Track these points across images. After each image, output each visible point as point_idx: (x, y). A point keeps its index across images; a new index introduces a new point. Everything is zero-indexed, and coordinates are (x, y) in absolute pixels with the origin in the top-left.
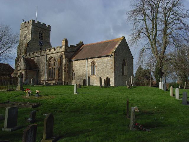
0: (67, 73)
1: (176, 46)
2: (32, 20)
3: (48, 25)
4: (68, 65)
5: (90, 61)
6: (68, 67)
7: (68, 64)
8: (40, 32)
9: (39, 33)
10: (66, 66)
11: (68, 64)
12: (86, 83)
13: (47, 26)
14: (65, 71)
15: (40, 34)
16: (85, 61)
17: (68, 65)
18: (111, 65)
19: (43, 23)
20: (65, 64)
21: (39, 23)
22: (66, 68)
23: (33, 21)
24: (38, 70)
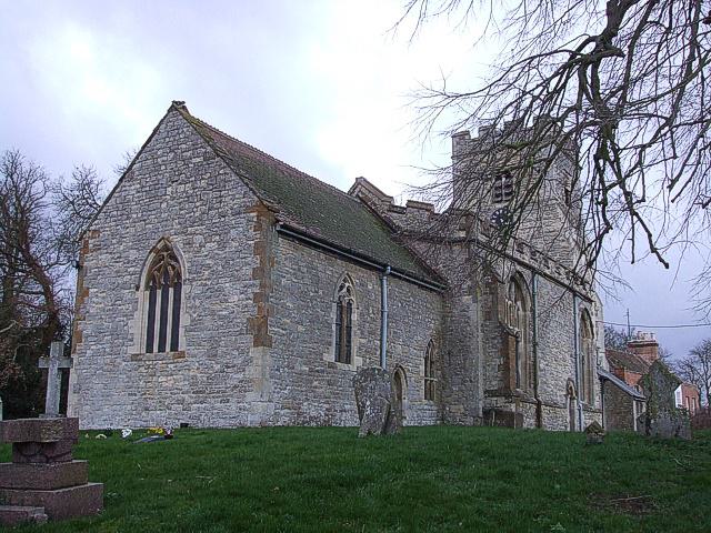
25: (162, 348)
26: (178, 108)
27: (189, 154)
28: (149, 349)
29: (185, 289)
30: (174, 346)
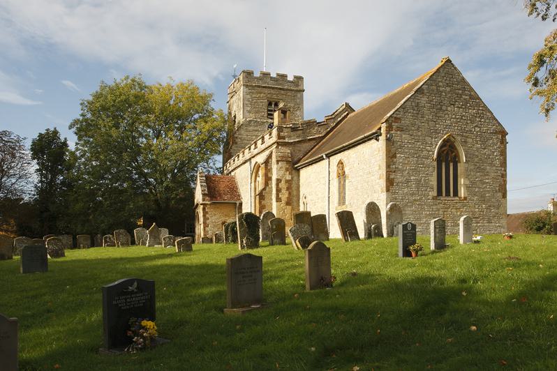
0: (288, 203)
1: (412, 214)
2: (243, 72)
3: (295, 77)
4: (287, 181)
5: (335, 159)
6: (288, 189)
7: (288, 177)
8: (270, 100)
9: (267, 104)
10: (283, 185)
11: (288, 177)
12: (297, 241)
13: (290, 78)
14: (278, 199)
15: (270, 104)
16: (325, 162)
17: (287, 181)
18: (379, 166)
19: (278, 75)
20: (279, 181)
21: (266, 75)
22: (284, 191)
23: (248, 74)
24: (238, 202)
25: (448, 194)
26: (449, 61)
27: (460, 92)
28: (439, 193)
29: (461, 168)
30: (456, 194)
